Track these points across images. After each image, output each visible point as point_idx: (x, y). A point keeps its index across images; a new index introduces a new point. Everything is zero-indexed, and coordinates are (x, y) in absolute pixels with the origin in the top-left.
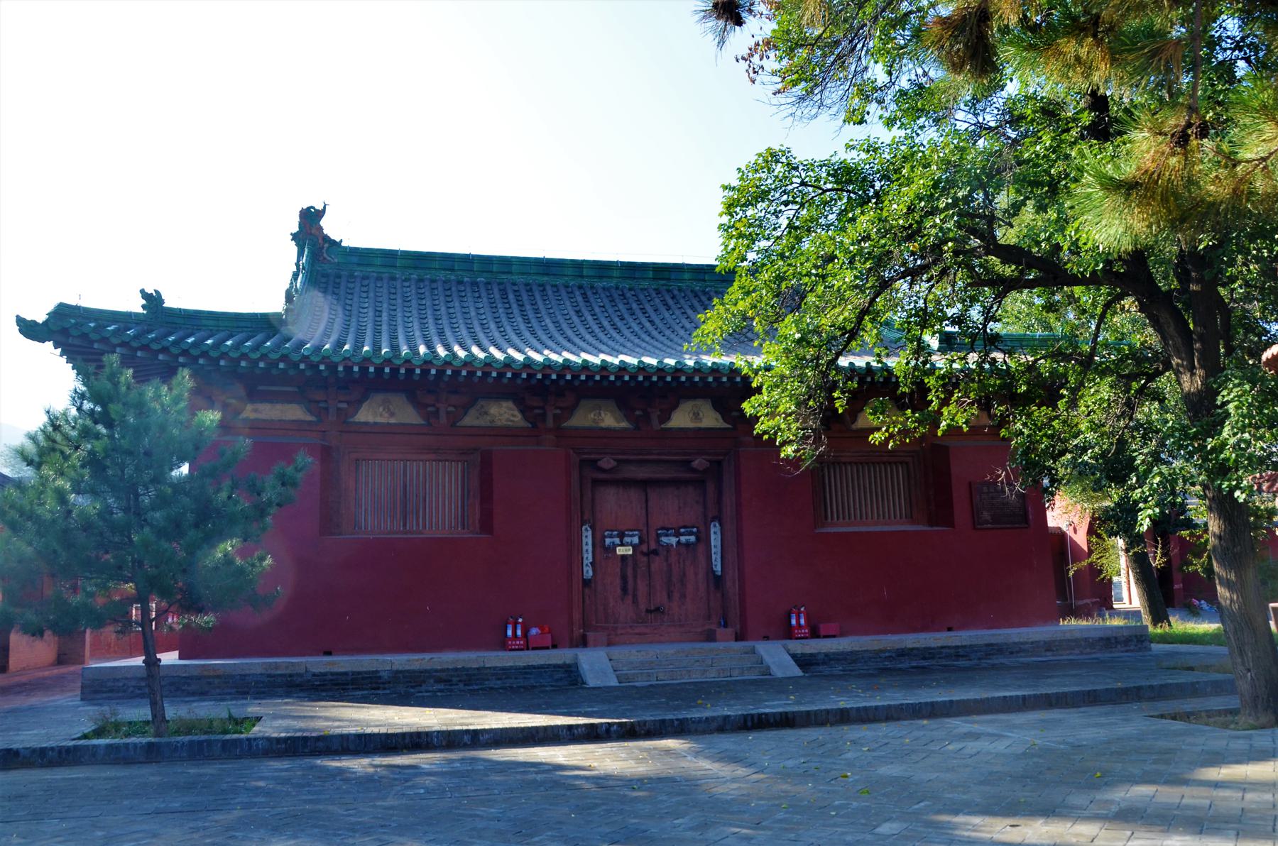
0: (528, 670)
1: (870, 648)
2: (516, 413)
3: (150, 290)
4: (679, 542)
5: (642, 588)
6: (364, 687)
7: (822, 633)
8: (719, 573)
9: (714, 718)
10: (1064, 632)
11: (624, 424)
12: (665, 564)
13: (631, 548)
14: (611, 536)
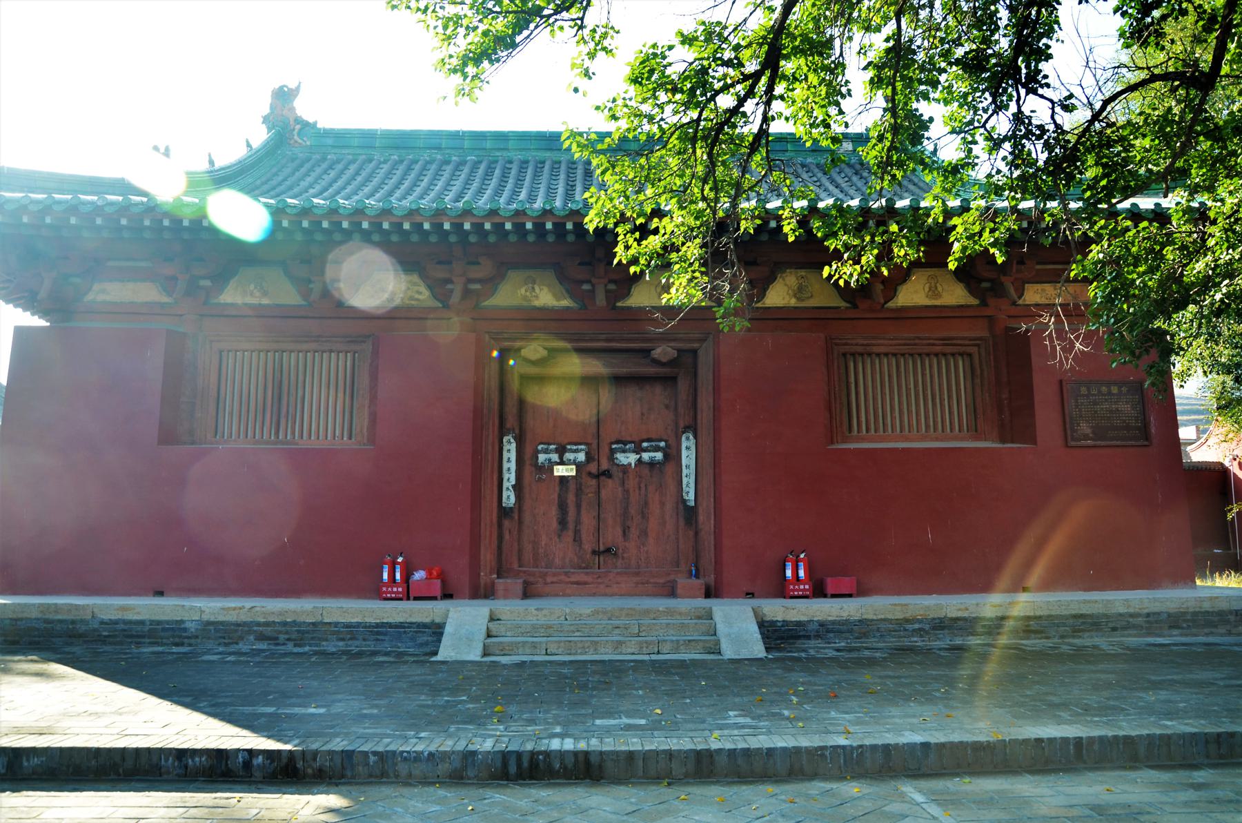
0: (379, 630)
1: (890, 616)
2: (423, 289)
4: (640, 461)
5: (588, 520)
6: (164, 641)
7: (830, 591)
8: (692, 504)
9: (445, 756)
10: (1201, 600)
11: (566, 302)
13: (574, 467)
14: (546, 451)
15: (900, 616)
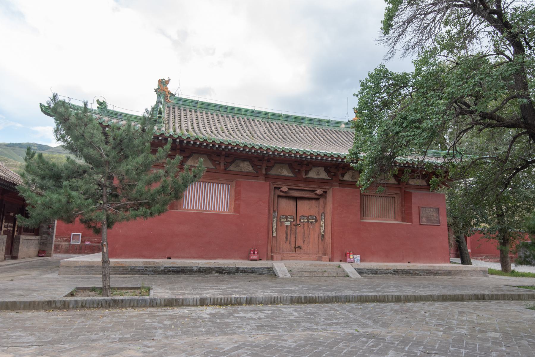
2: (250, 167)
3: (101, 101)
11: (291, 175)
12: (302, 229)
15: (385, 268)
